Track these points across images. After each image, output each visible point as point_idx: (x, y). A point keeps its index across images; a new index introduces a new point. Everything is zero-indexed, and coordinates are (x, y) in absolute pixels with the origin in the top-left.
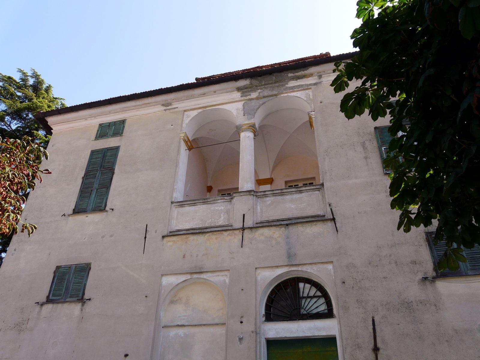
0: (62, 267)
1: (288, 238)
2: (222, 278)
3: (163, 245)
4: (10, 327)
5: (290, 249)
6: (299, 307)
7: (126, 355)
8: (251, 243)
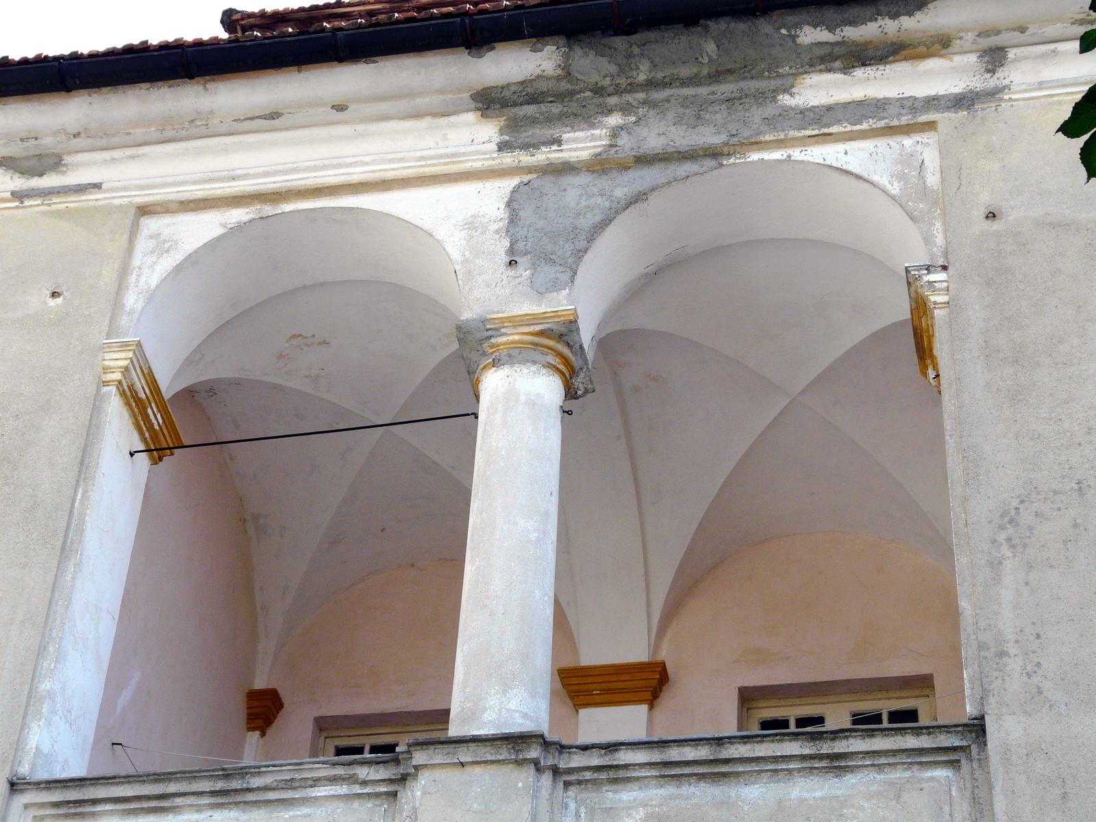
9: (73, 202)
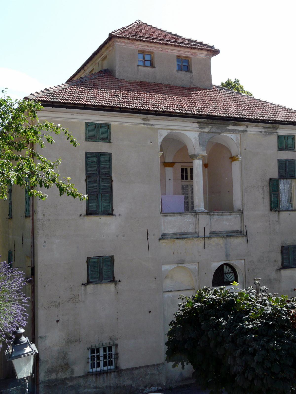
0: (92, 258)
1: (226, 244)
2: (194, 267)
3: (160, 245)
4: (66, 300)
5: (227, 251)
6: (223, 278)
7: (150, 312)
8: (209, 247)
9: (150, 126)
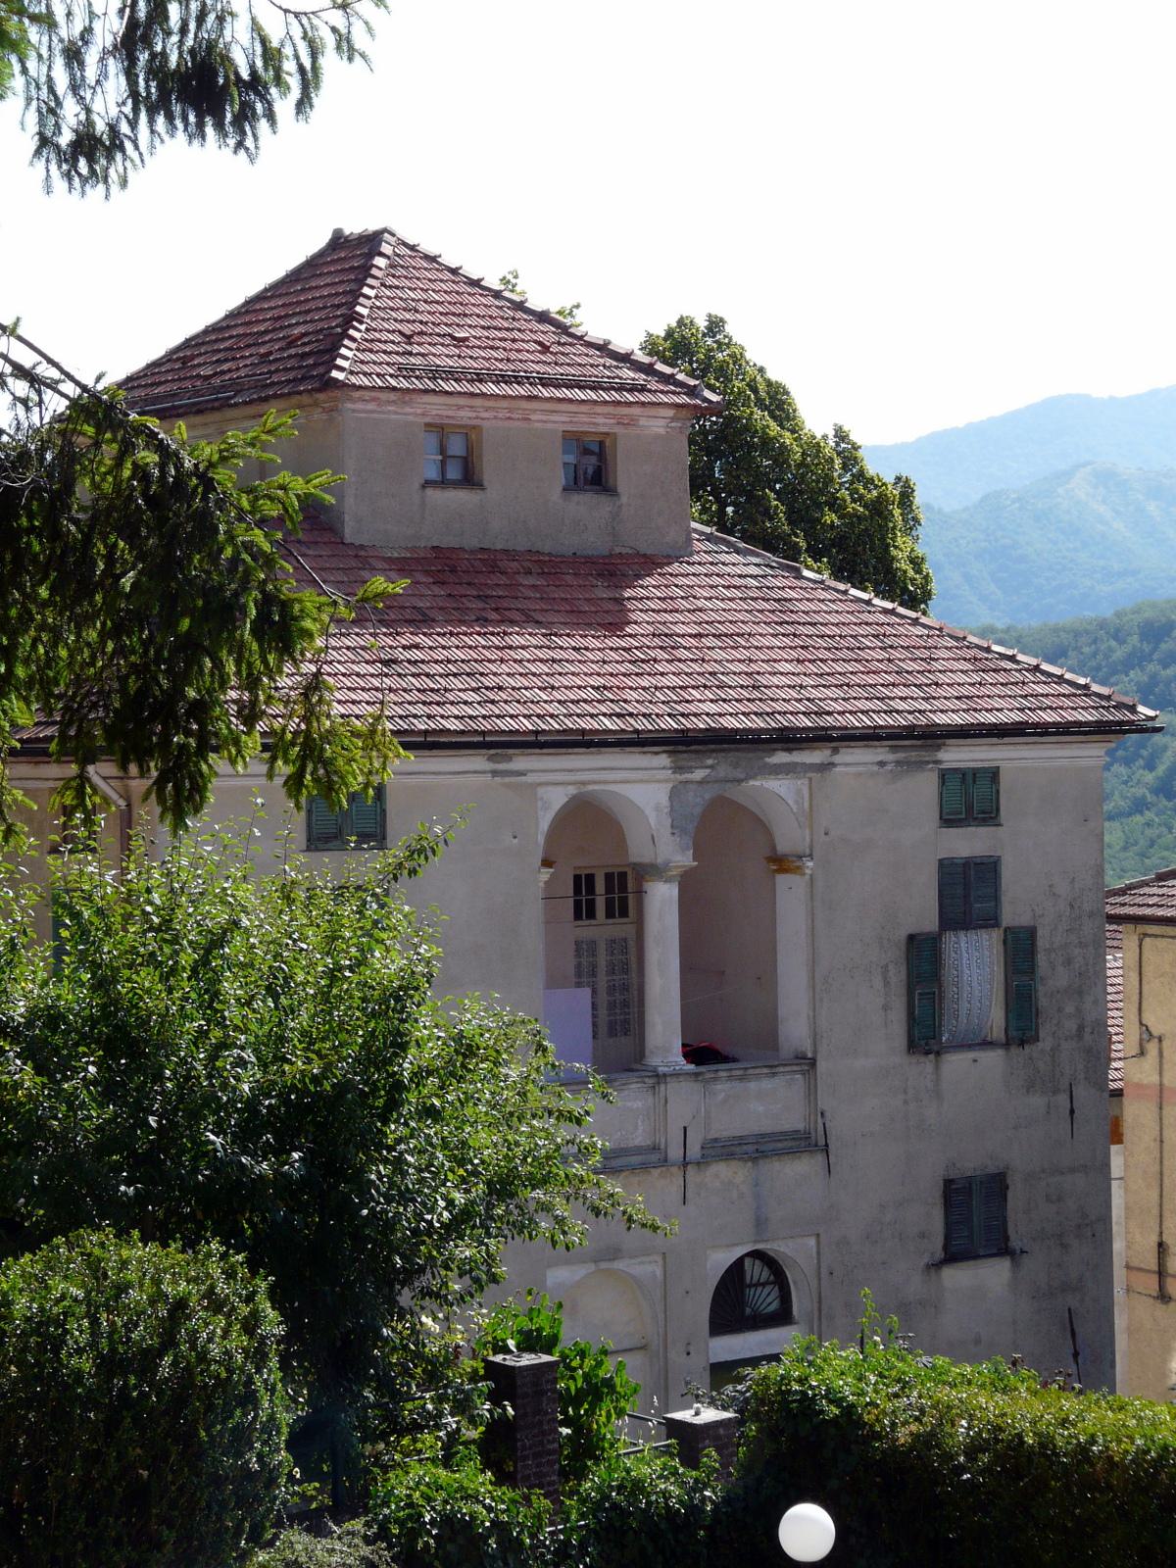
1: (757, 1185)
2: (649, 1268)
8: (699, 1195)
